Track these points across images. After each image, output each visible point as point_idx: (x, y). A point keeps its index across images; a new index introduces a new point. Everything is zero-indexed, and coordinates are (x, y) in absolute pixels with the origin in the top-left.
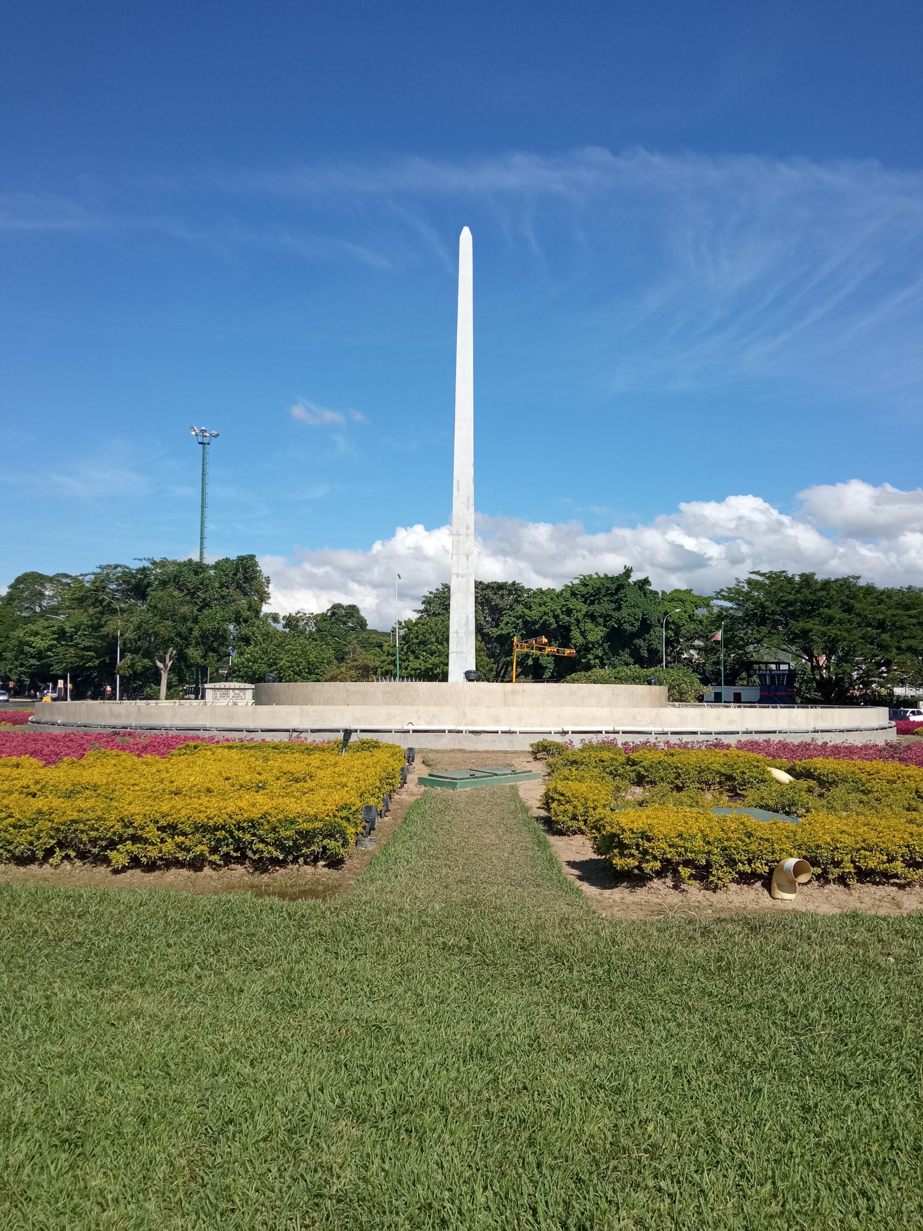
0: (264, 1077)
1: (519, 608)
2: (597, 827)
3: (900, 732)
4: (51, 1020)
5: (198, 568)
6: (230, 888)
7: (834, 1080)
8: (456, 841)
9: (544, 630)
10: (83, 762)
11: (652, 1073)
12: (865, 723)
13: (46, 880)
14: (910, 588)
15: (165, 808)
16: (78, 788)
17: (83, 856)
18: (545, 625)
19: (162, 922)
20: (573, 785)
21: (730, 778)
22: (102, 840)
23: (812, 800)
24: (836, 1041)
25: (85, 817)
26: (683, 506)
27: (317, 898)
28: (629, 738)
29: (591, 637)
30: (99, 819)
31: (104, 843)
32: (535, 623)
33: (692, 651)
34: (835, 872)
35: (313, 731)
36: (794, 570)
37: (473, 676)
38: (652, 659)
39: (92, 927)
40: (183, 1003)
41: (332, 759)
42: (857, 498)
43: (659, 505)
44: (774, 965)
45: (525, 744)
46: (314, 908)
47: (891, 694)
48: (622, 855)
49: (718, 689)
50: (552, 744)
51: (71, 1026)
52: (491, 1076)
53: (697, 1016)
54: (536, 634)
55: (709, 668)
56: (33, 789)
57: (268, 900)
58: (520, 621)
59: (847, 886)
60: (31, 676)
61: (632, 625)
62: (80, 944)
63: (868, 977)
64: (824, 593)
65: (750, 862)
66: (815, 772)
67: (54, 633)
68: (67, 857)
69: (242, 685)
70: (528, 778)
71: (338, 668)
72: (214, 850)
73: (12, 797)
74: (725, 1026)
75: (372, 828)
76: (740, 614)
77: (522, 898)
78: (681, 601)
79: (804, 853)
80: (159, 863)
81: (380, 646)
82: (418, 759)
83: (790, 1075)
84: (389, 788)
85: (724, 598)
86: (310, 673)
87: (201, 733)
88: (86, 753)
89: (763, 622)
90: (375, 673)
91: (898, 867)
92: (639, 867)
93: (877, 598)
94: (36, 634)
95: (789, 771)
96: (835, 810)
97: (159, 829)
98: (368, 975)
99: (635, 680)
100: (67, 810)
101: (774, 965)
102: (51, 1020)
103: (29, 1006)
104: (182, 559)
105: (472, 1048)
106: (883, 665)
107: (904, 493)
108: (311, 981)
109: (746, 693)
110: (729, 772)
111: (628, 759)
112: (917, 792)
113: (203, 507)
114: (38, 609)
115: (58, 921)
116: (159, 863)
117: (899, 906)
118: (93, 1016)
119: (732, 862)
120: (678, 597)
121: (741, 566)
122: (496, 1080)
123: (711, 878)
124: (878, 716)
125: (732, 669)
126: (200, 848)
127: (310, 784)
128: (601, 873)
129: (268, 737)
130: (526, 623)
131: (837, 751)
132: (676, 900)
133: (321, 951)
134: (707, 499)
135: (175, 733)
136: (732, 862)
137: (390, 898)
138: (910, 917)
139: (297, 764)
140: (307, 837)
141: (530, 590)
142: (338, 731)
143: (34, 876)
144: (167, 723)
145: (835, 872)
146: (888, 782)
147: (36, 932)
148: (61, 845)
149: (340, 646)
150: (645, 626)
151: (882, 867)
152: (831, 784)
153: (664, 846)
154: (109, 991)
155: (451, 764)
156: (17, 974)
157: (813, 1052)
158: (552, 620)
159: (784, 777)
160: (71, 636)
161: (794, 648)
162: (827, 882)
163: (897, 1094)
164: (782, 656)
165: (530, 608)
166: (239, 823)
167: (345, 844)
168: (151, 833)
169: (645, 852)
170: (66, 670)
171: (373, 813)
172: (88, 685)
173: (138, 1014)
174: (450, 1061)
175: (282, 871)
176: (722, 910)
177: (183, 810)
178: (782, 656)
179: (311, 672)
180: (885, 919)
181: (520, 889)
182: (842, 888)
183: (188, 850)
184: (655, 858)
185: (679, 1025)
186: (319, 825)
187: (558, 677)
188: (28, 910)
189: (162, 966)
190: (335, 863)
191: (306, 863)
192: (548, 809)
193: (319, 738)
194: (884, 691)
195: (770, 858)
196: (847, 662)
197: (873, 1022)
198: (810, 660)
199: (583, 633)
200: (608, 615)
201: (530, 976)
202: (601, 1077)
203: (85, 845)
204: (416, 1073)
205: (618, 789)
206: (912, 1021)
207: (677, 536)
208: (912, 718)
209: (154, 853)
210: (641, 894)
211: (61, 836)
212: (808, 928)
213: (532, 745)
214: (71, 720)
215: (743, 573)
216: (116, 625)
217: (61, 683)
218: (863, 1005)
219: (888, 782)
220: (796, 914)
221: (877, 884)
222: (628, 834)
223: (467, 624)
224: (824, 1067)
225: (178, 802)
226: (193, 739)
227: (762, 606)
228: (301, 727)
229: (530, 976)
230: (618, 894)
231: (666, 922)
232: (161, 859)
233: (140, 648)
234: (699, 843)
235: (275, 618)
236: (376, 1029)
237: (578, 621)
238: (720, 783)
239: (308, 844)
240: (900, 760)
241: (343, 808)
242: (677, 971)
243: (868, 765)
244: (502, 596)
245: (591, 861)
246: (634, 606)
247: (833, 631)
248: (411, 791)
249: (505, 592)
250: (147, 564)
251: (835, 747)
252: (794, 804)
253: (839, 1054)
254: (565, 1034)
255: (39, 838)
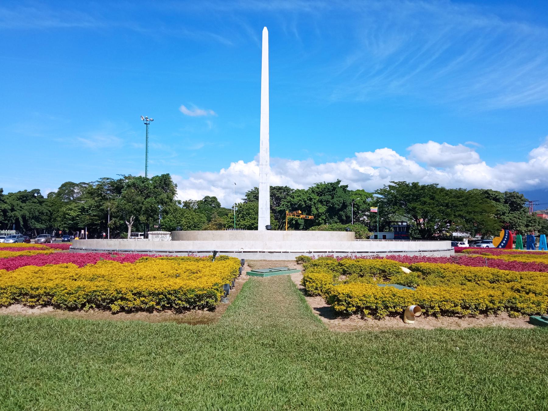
0: (187, 401)
1: (289, 198)
2: (327, 292)
3: (456, 251)
4: (90, 377)
5: (144, 180)
6: (165, 320)
7: (436, 400)
8: (264, 299)
9: (300, 207)
10: (96, 265)
11: (357, 397)
12: (440, 248)
13: (82, 317)
14: (460, 189)
15: (136, 285)
16: (96, 277)
17: (98, 306)
18: (300, 206)
19: (137, 335)
20: (316, 275)
21: (384, 271)
22: (107, 299)
23: (420, 281)
24: (436, 383)
25: (100, 289)
26: (357, 154)
27: (205, 324)
28: (339, 254)
29: (320, 211)
30: (106, 290)
31: (108, 301)
32: (295, 204)
33: (365, 217)
34: (431, 311)
35: (198, 252)
36: (409, 181)
37: (269, 228)
38: (347, 221)
39: (105, 337)
40: (148, 370)
41: (208, 264)
42: (433, 149)
43: (348, 153)
44: (407, 351)
45: (293, 257)
46: (204, 329)
47: (451, 235)
48: (338, 304)
49: (376, 234)
50: (305, 257)
51: (99, 380)
52: (287, 399)
53: (375, 373)
54: (296, 209)
55: (372, 224)
56: (75, 277)
57: (183, 325)
58: (289, 204)
59: (436, 317)
60: (69, 228)
61: (339, 205)
62: (100, 345)
63: (448, 356)
64: (422, 191)
65: (394, 307)
66: (420, 269)
67: (79, 209)
68: (92, 307)
69: (165, 232)
70: (295, 272)
71: (208, 224)
72: (158, 304)
73: (66, 281)
74: (388, 377)
75: (228, 294)
76: (385, 200)
77: (296, 324)
78: (359, 194)
79: (418, 303)
80: (133, 309)
81: (227, 215)
82: (246, 264)
83: (417, 397)
84: (234, 277)
85: (379, 193)
86: (195, 227)
87: (148, 253)
88: (98, 262)
89: (395, 204)
90: (225, 227)
91: (459, 309)
92: (346, 310)
93: (446, 193)
94: (71, 209)
95: (410, 268)
96: (430, 285)
97: (133, 294)
98: (230, 357)
99: (340, 229)
100: (92, 286)
101: (407, 351)
102: (90, 377)
103: (79, 372)
104: (138, 176)
105: (278, 387)
106: (448, 223)
107: (454, 147)
108: (205, 359)
109: (388, 235)
110: (383, 269)
111: (339, 263)
112: (465, 277)
113: (146, 152)
114: (72, 198)
115: (90, 335)
116: (133, 309)
117: (459, 326)
118: (109, 375)
119: (386, 307)
120: (359, 193)
121: (385, 180)
122: (289, 401)
123: (378, 314)
124: (447, 244)
125: (382, 224)
126: (152, 303)
127: (199, 274)
128: (329, 313)
129: (179, 255)
130: (291, 204)
131: (429, 260)
132: (362, 324)
133: (208, 347)
134: (367, 151)
135: (137, 253)
136: (386, 307)
137: (237, 324)
138: (465, 330)
139: (193, 266)
140: (199, 297)
141: (293, 190)
142: (210, 252)
143: (77, 316)
144: (133, 249)
145: (431, 311)
146: (453, 272)
147: (80, 340)
148: (89, 302)
149: (209, 214)
150: (344, 206)
151: (452, 309)
152: (428, 274)
153: (357, 300)
154: (115, 365)
155: (261, 266)
156: (73, 358)
157: (426, 388)
158: (303, 203)
159: (408, 271)
160: (87, 211)
161: (409, 215)
162: (428, 315)
163: (464, 405)
164: (404, 219)
165: (293, 198)
166: (169, 291)
167: (216, 300)
168: (130, 296)
169: (349, 303)
170: (85, 226)
171: (228, 287)
172: (95, 232)
173: (129, 375)
174: (268, 393)
175: (188, 312)
176: (383, 328)
177: (144, 286)
178: (404, 219)
179: (196, 227)
180: (454, 331)
181: (294, 320)
182: (434, 318)
183: (146, 304)
184: (353, 306)
185: (367, 377)
186: (205, 292)
187: (306, 228)
188: (76, 330)
189: (138, 354)
190: (212, 309)
191: (199, 309)
192: (305, 285)
193: (201, 255)
194: (448, 234)
195: (403, 305)
196: (432, 221)
197: (452, 375)
198: (416, 221)
199: (317, 209)
200: (328, 201)
201: (301, 357)
202: (335, 399)
203: (100, 301)
204: (254, 398)
205: (335, 276)
206: (468, 374)
207: (355, 165)
208: (460, 246)
209: (131, 305)
210: (347, 322)
211: (89, 298)
212: (422, 335)
213: (296, 258)
214: (89, 248)
215: (387, 182)
216: (107, 205)
217: (83, 232)
218: (447, 368)
219: (453, 272)
220: (415, 329)
221: (450, 316)
222: (341, 295)
223: (266, 204)
224: (431, 394)
225: (141, 282)
226: (145, 255)
227: (395, 197)
228: (193, 250)
229: (301, 357)
230: (337, 322)
231: (359, 333)
232: (134, 308)
233: (118, 216)
234: (372, 299)
235: (179, 202)
236: (235, 380)
237: (314, 203)
238: (379, 273)
239: (199, 301)
240: (457, 263)
241: (215, 285)
242: (365, 354)
243: (444, 265)
244: (281, 193)
245: (324, 307)
246: (339, 197)
247: (426, 208)
248: (243, 278)
249: (282, 191)
250: (122, 178)
251: (429, 258)
252: (412, 282)
253: (438, 388)
254: (318, 381)
255: (79, 299)
